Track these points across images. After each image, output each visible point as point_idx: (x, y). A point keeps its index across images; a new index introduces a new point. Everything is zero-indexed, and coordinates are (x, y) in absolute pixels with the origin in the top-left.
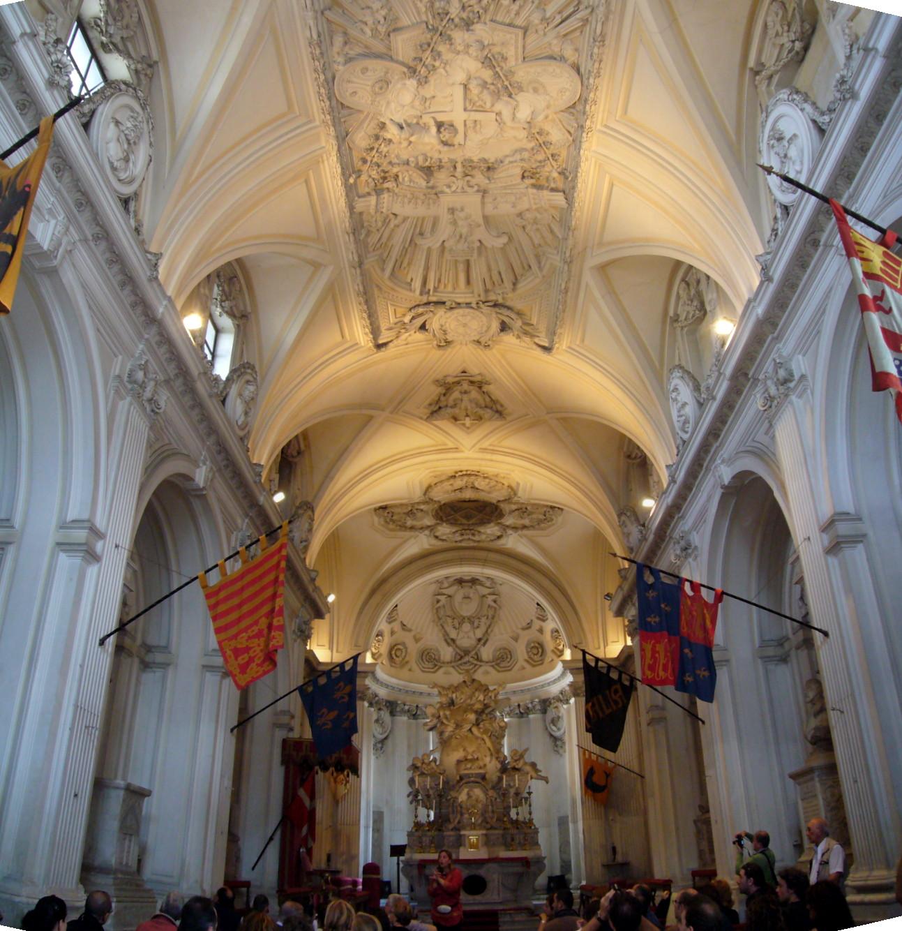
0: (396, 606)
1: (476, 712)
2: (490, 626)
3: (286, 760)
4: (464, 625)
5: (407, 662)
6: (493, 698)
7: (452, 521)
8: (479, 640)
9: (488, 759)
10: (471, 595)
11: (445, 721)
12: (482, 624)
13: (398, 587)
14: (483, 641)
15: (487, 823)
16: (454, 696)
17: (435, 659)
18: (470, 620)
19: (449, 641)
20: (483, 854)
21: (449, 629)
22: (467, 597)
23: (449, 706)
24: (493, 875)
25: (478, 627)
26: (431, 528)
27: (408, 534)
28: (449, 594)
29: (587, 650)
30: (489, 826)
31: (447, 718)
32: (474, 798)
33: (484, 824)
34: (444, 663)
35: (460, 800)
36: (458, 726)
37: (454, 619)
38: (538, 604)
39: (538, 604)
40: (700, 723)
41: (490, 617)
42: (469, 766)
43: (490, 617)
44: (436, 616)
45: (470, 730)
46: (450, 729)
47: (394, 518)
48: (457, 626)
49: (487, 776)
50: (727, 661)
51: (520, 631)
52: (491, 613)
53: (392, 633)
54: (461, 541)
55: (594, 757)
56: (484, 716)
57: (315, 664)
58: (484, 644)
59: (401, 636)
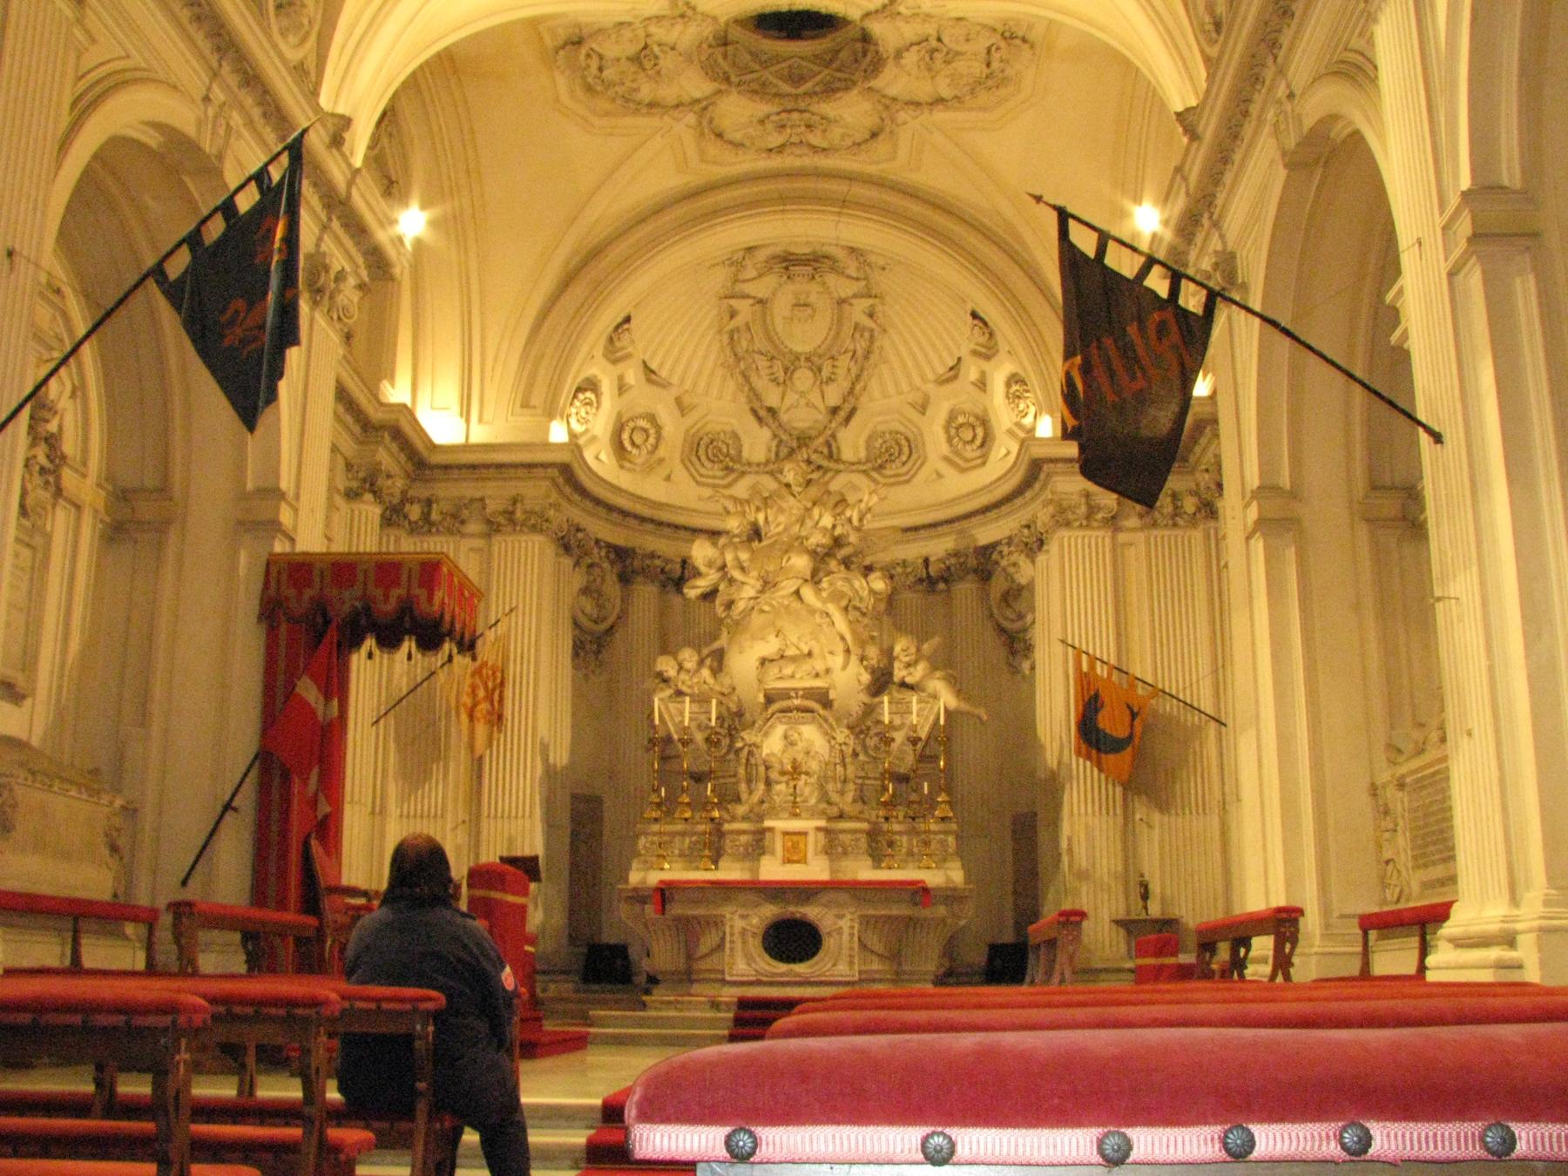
0: (628, 320)
1: (813, 553)
2: (858, 377)
3: (271, 611)
4: (797, 375)
5: (661, 461)
6: (855, 522)
7: (755, 86)
8: (834, 411)
9: (838, 660)
10: (813, 299)
11: (737, 574)
12: (841, 372)
13: (625, 266)
14: (843, 414)
15: (829, 803)
16: (761, 517)
17: (728, 455)
18: (812, 362)
19: (762, 413)
20: (816, 869)
21: (761, 383)
22: (801, 305)
23: (750, 540)
24: (839, 927)
25: (830, 380)
26: (703, 107)
27: (644, 122)
28: (760, 295)
29: (1071, 209)
30: (834, 811)
31: (743, 569)
32: (801, 745)
33: (823, 806)
34: (749, 464)
35: (765, 751)
36: (768, 584)
37: (772, 358)
38: (975, 315)
39: (975, 315)
40: (1424, 437)
41: (860, 353)
42: (788, 671)
43: (860, 353)
44: (728, 351)
45: (797, 593)
46: (749, 592)
47: (606, 73)
48: (781, 375)
49: (832, 695)
50: (1535, 235)
51: (930, 388)
52: (861, 345)
53: (622, 388)
54: (781, 149)
55: (1101, 670)
56: (833, 564)
57: (419, 445)
58: (848, 419)
59: (644, 398)
